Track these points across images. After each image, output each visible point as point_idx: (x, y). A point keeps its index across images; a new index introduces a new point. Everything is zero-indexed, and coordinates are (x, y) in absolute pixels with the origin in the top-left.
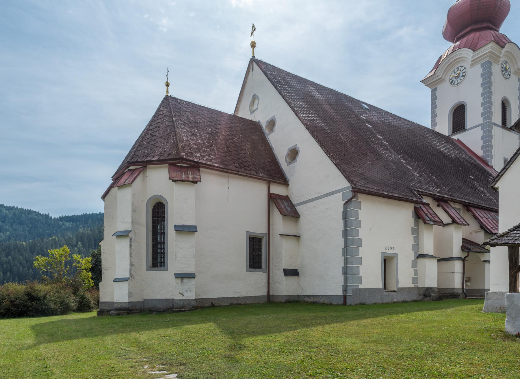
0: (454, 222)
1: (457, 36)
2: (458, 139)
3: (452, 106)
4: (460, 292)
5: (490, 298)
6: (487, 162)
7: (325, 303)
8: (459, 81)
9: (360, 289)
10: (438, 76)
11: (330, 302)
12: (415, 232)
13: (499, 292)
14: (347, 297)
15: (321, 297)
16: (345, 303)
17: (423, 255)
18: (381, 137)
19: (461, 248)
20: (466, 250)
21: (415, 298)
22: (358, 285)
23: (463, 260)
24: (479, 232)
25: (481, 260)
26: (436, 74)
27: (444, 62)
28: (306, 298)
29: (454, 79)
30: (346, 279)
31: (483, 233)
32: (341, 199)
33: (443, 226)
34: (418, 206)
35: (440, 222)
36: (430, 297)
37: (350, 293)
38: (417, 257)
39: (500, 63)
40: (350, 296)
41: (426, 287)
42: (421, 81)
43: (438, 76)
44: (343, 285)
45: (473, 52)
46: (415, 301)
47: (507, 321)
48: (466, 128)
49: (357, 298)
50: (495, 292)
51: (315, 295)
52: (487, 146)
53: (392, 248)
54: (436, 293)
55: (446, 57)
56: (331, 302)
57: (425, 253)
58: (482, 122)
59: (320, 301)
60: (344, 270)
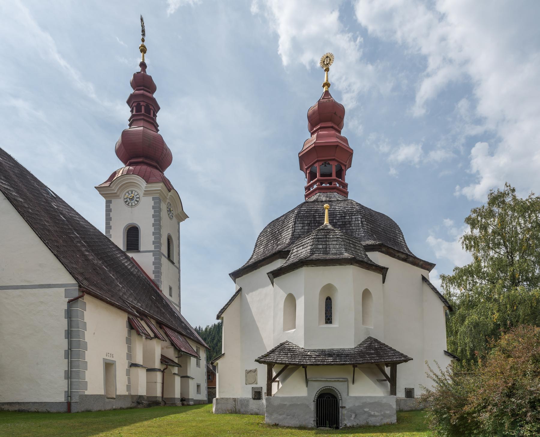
0: (156, 336)
1: (130, 161)
2: (132, 257)
3: (127, 225)
4: (160, 400)
5: (219, 403)
6: (158, 286)
7: (39, 411)
8: (133, 204)
9: (86, 395)
10: (113, 190)
11: (46, 410)
12: (129, 341)
13: (224, 398)
14: (72, 403)
15: (31, 403)
16: (69, 410)
17: (136, 364)
18: (79, 236)
19: (160, 361)
20: (164, 362)
21: (129, 405)
22: (84, 391)
23: (163, 372)
24: (170, 348)
25: (172, 372)
26: (111, 187)
27: (118, 180)
28: (5, 406)
29: (128, 199)
30: (70, 385)
31: (173, 349)
32: (63, 295)
33: (151, 339)
34: (131, 317)
35: (148, 335)
36: (143, 404)
37: (75, 399)
38: (131, 366)
39: (166, 203)
40: (76, 402)
41: (139, 395)
42: (95, 187)
43: (113, 190)
44: (67, 390)
45: (146, 183)
46: (131, 408)
47: (266, 416)
48: (139, 250)
49: (83, 405)
50: (222, 398)
51: (22, 401)
52: (158, 271)
53: (112, 355)
54: (146, 401)
55: (121, 176)
56: (49, 410)
57: (137, 363)
58: (153, 249)
59: (30, 409)
60: (68, 375)
